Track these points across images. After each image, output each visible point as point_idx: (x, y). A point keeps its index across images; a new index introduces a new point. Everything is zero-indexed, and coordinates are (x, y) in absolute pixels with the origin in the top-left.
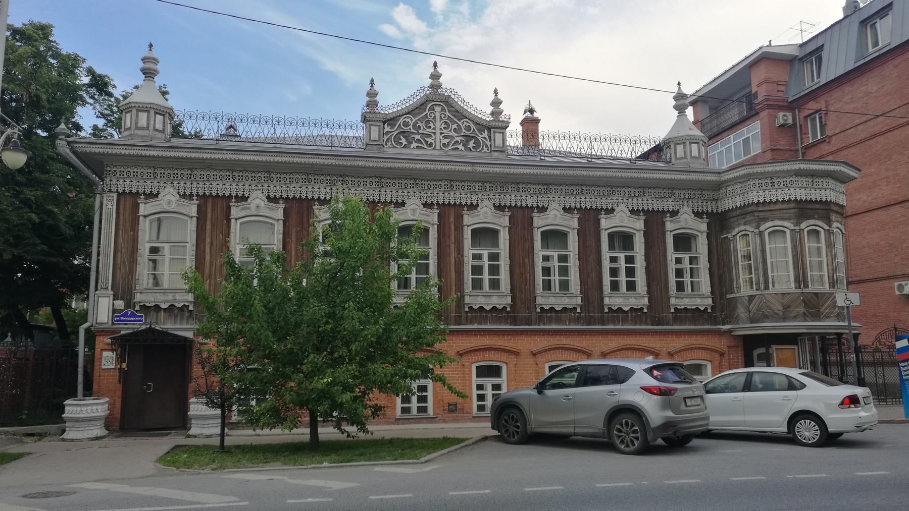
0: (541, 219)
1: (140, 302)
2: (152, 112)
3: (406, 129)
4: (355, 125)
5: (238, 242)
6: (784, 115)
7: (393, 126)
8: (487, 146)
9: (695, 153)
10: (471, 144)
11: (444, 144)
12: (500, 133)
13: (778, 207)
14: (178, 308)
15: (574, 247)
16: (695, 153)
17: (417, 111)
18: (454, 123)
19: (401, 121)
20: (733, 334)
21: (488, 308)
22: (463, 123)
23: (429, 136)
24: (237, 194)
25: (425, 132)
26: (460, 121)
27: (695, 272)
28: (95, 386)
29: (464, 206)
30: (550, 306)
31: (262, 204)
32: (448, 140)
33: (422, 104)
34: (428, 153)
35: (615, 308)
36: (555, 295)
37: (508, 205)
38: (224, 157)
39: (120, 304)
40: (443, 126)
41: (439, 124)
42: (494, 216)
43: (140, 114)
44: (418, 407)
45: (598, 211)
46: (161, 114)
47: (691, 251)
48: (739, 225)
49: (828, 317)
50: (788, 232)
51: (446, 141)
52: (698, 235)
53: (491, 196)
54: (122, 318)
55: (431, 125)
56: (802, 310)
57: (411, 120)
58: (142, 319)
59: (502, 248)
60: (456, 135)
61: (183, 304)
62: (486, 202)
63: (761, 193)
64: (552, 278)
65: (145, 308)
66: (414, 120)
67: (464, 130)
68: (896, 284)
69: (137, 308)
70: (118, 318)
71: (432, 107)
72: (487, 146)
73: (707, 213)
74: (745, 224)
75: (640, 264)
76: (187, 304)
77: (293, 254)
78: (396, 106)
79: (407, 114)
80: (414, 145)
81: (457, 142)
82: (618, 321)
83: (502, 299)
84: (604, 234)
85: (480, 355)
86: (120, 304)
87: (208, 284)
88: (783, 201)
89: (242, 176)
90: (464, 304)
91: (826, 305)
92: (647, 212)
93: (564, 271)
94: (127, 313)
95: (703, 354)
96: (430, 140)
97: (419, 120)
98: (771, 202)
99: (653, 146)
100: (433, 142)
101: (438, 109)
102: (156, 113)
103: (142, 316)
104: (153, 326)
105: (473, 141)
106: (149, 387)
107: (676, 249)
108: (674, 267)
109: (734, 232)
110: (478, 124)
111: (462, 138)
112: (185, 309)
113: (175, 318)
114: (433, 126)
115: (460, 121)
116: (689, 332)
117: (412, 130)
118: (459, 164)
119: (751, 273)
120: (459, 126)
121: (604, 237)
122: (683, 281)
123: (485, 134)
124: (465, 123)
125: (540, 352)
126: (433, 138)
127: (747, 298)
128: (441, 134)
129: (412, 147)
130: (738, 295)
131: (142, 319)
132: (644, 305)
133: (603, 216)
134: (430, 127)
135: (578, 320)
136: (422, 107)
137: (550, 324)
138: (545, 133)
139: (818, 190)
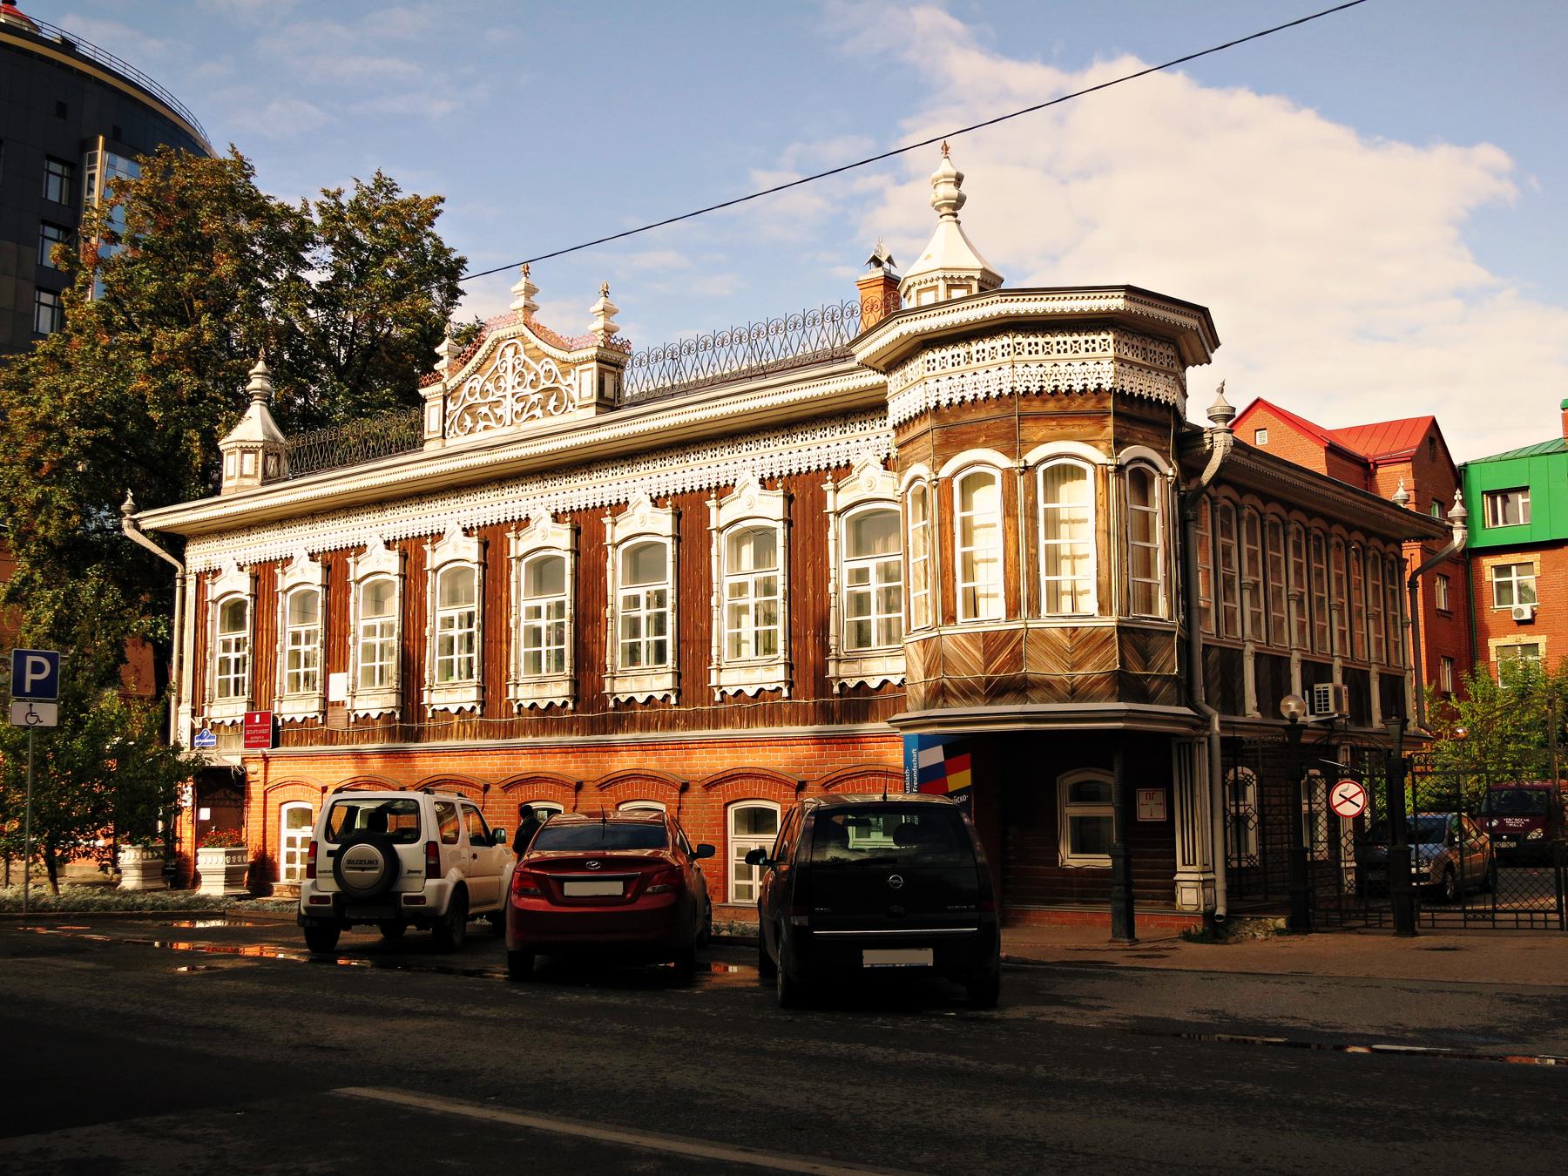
10: (552, 403)
27: (446, 648)
32: (522, 404)
34: (498, 434)
41: (510, 380)
43: (246, 455)
46: (250, 452)
50: (1090, 470)
80: (482, 424)
83: (558, 691)
96: (499, 411)
118: (568, 435)
119: (470, 650)
133: (829, 486)
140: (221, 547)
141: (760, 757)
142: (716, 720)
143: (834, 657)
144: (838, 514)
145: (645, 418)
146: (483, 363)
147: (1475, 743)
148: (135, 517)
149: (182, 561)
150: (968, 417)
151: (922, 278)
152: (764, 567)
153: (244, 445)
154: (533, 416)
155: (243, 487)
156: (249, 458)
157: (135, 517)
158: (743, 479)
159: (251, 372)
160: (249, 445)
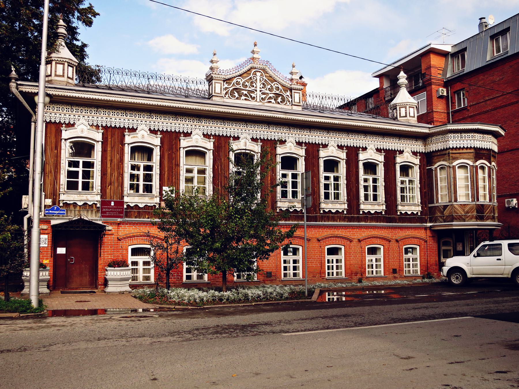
0: (324, 152)
1: (63, 201)
2: (66, 64)
3: (238, 87)
4: (129, 73)
5: (67, 157)
6: (442, 90)
7: (229, 84)
8: (289, 101)
9: (60, 72)
10: (279, 100)
11: (262, 98)
12: (297, 93)
13: (465, 151)
14: (90, 205)
15: (302, 168)
16: (60, 72)
17: (245, 75)
18: (269, 84)
19: (235, 80)
20: (432, 229)
21: (334, 211)
22: (274, 85)
23: (252, 92)
24: (129, 126)
25: (250, 89)
26: (272, 83)
28: (120, 258)
29: (63, 124)
30: (329, 209)
31: (145, 134)
32: (265, 96)
33: (249, 70)
35: (327, 211)
36: (332, 203)
37: (304, 142)
38: (124, 100)
39: (49, 202)
40: (262, 86)
41: (259, 85)
42: (296, 149)
43: (58, 65)
44: (144, 276)
45: (227, 138)
47: (91, 157)
48: (439, 161)
49: (487, 219)
51: (264, 96)
52: (340, 162)
53: (201, 127)
54: (50, 212)
55: (254, 85)
56: (475, 214)
57: (241, 81)
58: (64, 212)
59: (380, 175)
60: (270, 92)
61: (93, 202)
62: (82, 120)
63: (462, 141)
64: (330, 191)
65: (66, 205)
66: (243, 81)
67: (275, 90)
68: (506, 200)
69: (61, 204)
70: (48, 212)
71: (255, 73)
72: (289, 101)
73: (305, 143)
74: (443, 161)
75: (381, 184)
76: (96, 202)
77: (166, 170)
78: (232, 70)
79: (239, 76)
80: (243, 97)
81: (271, 97)
82: (368, 220)
83: (381, 207)
84: (278, 158)
85: (105, 240)
86: (49, 202)
87: (109, 189)
88: (467, 148)
89: (50, 107)
90: (59, 201)
91: (487, 212)
92: (386, 151)
93: (337, 187)
94: (54, 208)
95: (379, 241)
96: (253, 95)
97: (246, 81)
98: (460, 148)
99: (346, 102)
100: (255, 96)
101: (258, 74)
102: (68, 65)
103: (64, 211)
104: (82, 218)
105: (280, 97)
106: (72, 261)
107: (326, 170)
108: (185, 175)
109: (436, 166)
110: (284, 86)
111: (274, 95)
112: (94, 206)
113: (88, 211)
114: (255, 86)
115: (272, 83)
116: (408, 227)
117: (242, 88)
120: (271, 86)
121: (321, 163)
122: (89, 182)
123: (288, 93)
124: (276, 85)
125: (322, 239)
126: (256, 94)
127: (442, 207)
128: (260, 91)
129: (242, 99)
130: (437, 205)
131: (64, 212)
132: (156, 203)
134: (253, 86)
135: (344, 219)
136: (248, 72)
137: (328, 221)
138: (194, 80)
139: (486, 142)
140: (200, 123)
141: (377, 232)
142: (359, 220)
145: (359, 121)
146: (243, 74)
148: (19, 82)
150: (482, 152)
151: (410, 104)
154: (270, 102)
157: (19, 82)
158: (331, 144)
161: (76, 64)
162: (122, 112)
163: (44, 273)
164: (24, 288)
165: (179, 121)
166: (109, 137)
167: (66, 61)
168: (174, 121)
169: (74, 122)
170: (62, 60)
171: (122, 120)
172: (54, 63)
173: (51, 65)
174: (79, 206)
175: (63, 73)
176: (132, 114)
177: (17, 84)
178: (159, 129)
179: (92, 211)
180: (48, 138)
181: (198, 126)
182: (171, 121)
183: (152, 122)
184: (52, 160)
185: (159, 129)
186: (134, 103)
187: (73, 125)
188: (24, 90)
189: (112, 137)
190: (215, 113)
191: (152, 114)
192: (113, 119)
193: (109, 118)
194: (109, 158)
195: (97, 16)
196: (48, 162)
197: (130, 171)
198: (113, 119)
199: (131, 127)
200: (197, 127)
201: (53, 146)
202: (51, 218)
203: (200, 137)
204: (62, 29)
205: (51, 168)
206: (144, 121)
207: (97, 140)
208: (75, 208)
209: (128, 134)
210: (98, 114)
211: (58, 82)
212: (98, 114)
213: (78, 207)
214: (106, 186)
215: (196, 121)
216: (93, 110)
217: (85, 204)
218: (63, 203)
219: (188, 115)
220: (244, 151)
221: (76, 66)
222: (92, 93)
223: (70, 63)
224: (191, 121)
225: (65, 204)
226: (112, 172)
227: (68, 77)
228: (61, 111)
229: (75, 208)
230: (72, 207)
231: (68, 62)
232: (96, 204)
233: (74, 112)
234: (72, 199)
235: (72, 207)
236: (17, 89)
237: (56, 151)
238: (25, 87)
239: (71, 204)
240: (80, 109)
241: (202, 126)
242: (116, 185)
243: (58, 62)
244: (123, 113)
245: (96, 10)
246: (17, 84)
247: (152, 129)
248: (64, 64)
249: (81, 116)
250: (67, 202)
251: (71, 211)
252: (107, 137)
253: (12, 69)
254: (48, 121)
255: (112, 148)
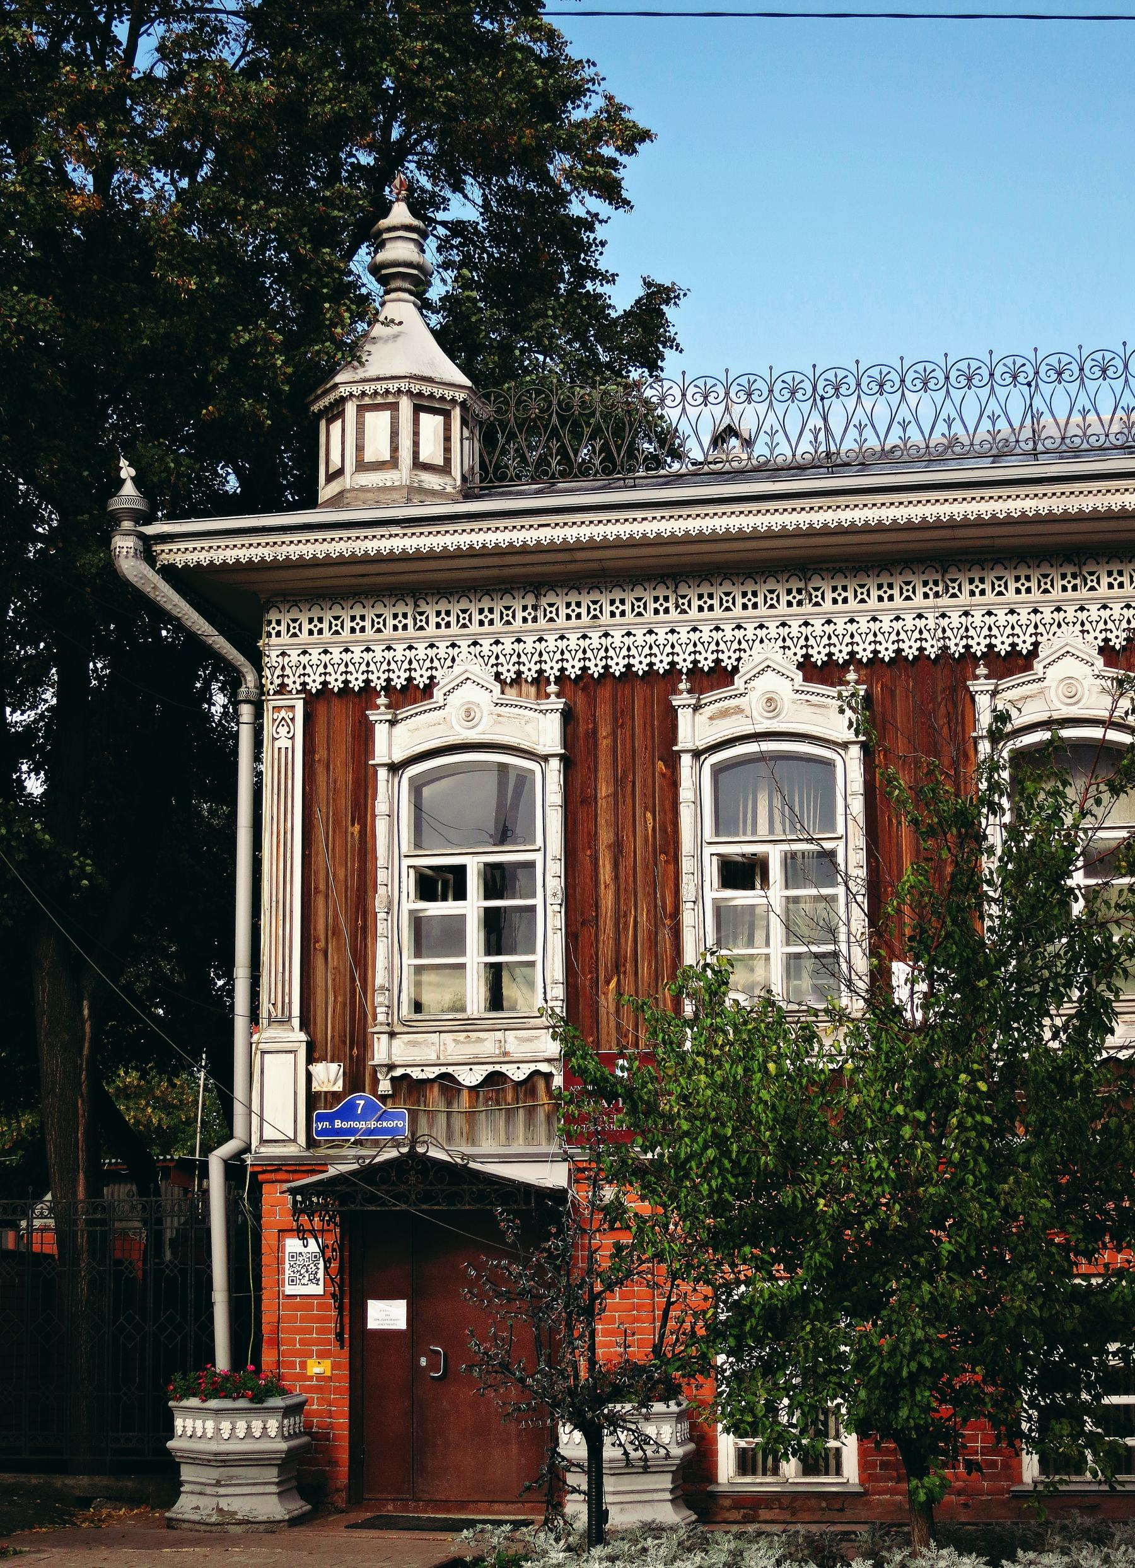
1: (391, 1067)
2: (406, 406)
38: (846, 517)
53: (1094, 612)
54: (338, 1124)
58: (400, 1124)
61: (533, 1067)
62: (469, 665)
69: (385, 1086)
76: (544, 1068)
87: (611, 996)
94: (352, 1106)
102: (418, 409)
112: (541, 1085)
131: (400, 1124)
140: (1083, 593)
143: (386, 1029)
144: (395, 768)
147: (176, 1219)
148: (151, 530)
149: (256, 659)
152: (737, 835)
153: (427, 389)
155: (422, 490)
156: (431, 424)
157: (151, 530)
158: (1057, 643)
159: (384, 223)
160: (438, 392)
161: (461, 396)
162: (661, 592)
163: (257, 1425)
164: (180, 1493)
165: (964, 598)
166: (604, 731)
167: (399, 391)
168: (711, 615)
169: (431, 678)
170: (380, 387)
171: (662, 632)
172: (351, 408)
173: (343, 422)
174: (471, 1089)
175: (395, 449)
176: (711, 596)
177: (142, 536)
178: (852, 654)
179: (531, 1111)
180: (320, 770)
181: (1070, 610)
182: (918, 600)
183: (818, 623)
184: (341, 874)
185: (852, 654)
186: (687, 540)
187: (427, 691)
188: (179, 560)
189: (616, 726)
190: (1041, 529)
191: (816, 582)
192: (617, 635)
193: (595, 635)
194: (605, 837)
195: (642, 148)
196: (322, 887)
197: (410, 903)
198: (617, 635)
199: (706, 665)
200: (1070, 612)
201: (345, 803)
202: (328, 1156)
203: (1087, 669)
204: (400, 244)
205: (335, 910)
206: (772, 625)
207: (542, 750)
208: (449, 1104)
209: (990, 685)
210: (542, 622)
211: (370, 495)
212: (542, 622)
213: (465, 1093)
214: (595, 982)
215: (920, 591)
216: (517, 606)
217: (495, 1079)
218: (393, 1079)
219: (649, 579)
220: (1096, 733)
221: (463, 404)
222: (476, 525)
223: (420, 395)
224: (1033, 584)
225: (405, 1085)
226: (623, 907)
227: (418, 465)
228: (370, 633)
229: (449, 1104)
230: (434, 1095)
231: (409, 392)
232: (548, 1076)
233: (431, 630)
234: (433, 1057)
235: (434, 1095)
236: (149, 558)
237: (357, 827)
238: (182, 546)
239: (428, 1080)
240: (455, 609)
241: (1093, 608)
242: (644, 970)
243: (367, 401)
244: (666, 599)
245: (639, 116)
246: (142, 536)
247: (819, 658)
248: (394, 407)
249: (464, 644)
250: (409, 1071)
251: (431, 1115)
252: (595, 731)
253: (123, 474)
254: (314, 687)
255: (618, 782)
